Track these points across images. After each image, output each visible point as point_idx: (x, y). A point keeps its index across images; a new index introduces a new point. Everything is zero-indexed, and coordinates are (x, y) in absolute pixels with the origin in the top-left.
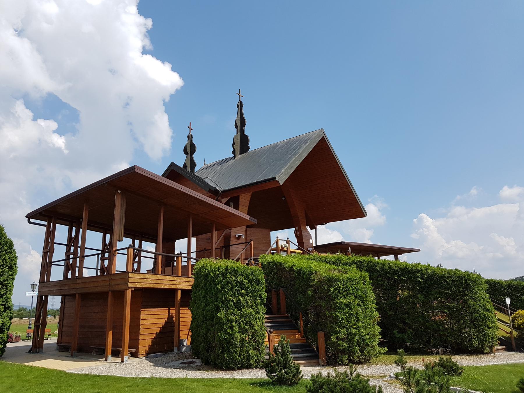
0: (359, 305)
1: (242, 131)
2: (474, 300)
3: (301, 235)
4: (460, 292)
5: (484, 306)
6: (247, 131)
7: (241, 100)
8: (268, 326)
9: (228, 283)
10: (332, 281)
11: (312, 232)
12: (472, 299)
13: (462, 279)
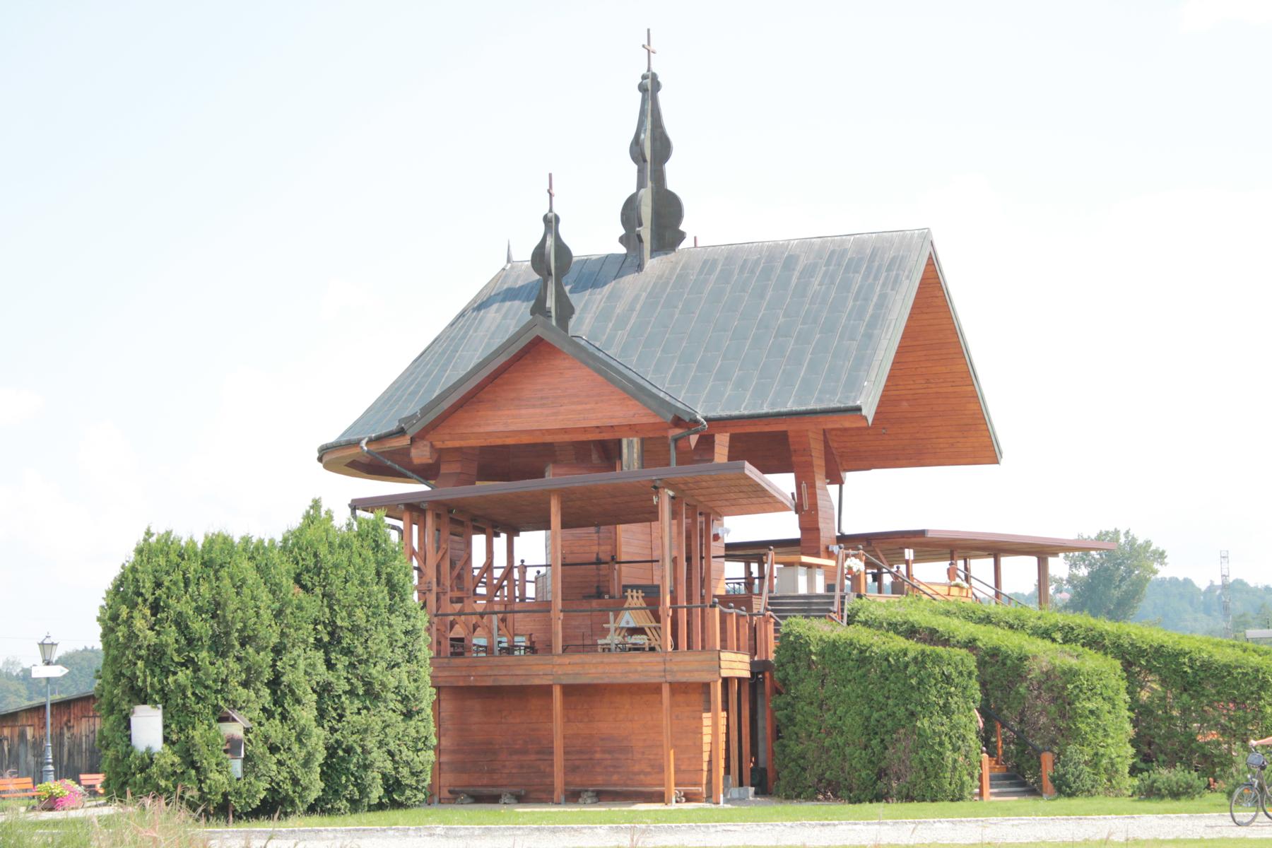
0: (1109, 712)
1: (659, 178)
3: (814, 506)
6: (676, 177)
7: (654, 69)
8: (646, 774)
9: (929, 676)
10: (1072, 674)
11: (833, 489)
13: (1257, 671)
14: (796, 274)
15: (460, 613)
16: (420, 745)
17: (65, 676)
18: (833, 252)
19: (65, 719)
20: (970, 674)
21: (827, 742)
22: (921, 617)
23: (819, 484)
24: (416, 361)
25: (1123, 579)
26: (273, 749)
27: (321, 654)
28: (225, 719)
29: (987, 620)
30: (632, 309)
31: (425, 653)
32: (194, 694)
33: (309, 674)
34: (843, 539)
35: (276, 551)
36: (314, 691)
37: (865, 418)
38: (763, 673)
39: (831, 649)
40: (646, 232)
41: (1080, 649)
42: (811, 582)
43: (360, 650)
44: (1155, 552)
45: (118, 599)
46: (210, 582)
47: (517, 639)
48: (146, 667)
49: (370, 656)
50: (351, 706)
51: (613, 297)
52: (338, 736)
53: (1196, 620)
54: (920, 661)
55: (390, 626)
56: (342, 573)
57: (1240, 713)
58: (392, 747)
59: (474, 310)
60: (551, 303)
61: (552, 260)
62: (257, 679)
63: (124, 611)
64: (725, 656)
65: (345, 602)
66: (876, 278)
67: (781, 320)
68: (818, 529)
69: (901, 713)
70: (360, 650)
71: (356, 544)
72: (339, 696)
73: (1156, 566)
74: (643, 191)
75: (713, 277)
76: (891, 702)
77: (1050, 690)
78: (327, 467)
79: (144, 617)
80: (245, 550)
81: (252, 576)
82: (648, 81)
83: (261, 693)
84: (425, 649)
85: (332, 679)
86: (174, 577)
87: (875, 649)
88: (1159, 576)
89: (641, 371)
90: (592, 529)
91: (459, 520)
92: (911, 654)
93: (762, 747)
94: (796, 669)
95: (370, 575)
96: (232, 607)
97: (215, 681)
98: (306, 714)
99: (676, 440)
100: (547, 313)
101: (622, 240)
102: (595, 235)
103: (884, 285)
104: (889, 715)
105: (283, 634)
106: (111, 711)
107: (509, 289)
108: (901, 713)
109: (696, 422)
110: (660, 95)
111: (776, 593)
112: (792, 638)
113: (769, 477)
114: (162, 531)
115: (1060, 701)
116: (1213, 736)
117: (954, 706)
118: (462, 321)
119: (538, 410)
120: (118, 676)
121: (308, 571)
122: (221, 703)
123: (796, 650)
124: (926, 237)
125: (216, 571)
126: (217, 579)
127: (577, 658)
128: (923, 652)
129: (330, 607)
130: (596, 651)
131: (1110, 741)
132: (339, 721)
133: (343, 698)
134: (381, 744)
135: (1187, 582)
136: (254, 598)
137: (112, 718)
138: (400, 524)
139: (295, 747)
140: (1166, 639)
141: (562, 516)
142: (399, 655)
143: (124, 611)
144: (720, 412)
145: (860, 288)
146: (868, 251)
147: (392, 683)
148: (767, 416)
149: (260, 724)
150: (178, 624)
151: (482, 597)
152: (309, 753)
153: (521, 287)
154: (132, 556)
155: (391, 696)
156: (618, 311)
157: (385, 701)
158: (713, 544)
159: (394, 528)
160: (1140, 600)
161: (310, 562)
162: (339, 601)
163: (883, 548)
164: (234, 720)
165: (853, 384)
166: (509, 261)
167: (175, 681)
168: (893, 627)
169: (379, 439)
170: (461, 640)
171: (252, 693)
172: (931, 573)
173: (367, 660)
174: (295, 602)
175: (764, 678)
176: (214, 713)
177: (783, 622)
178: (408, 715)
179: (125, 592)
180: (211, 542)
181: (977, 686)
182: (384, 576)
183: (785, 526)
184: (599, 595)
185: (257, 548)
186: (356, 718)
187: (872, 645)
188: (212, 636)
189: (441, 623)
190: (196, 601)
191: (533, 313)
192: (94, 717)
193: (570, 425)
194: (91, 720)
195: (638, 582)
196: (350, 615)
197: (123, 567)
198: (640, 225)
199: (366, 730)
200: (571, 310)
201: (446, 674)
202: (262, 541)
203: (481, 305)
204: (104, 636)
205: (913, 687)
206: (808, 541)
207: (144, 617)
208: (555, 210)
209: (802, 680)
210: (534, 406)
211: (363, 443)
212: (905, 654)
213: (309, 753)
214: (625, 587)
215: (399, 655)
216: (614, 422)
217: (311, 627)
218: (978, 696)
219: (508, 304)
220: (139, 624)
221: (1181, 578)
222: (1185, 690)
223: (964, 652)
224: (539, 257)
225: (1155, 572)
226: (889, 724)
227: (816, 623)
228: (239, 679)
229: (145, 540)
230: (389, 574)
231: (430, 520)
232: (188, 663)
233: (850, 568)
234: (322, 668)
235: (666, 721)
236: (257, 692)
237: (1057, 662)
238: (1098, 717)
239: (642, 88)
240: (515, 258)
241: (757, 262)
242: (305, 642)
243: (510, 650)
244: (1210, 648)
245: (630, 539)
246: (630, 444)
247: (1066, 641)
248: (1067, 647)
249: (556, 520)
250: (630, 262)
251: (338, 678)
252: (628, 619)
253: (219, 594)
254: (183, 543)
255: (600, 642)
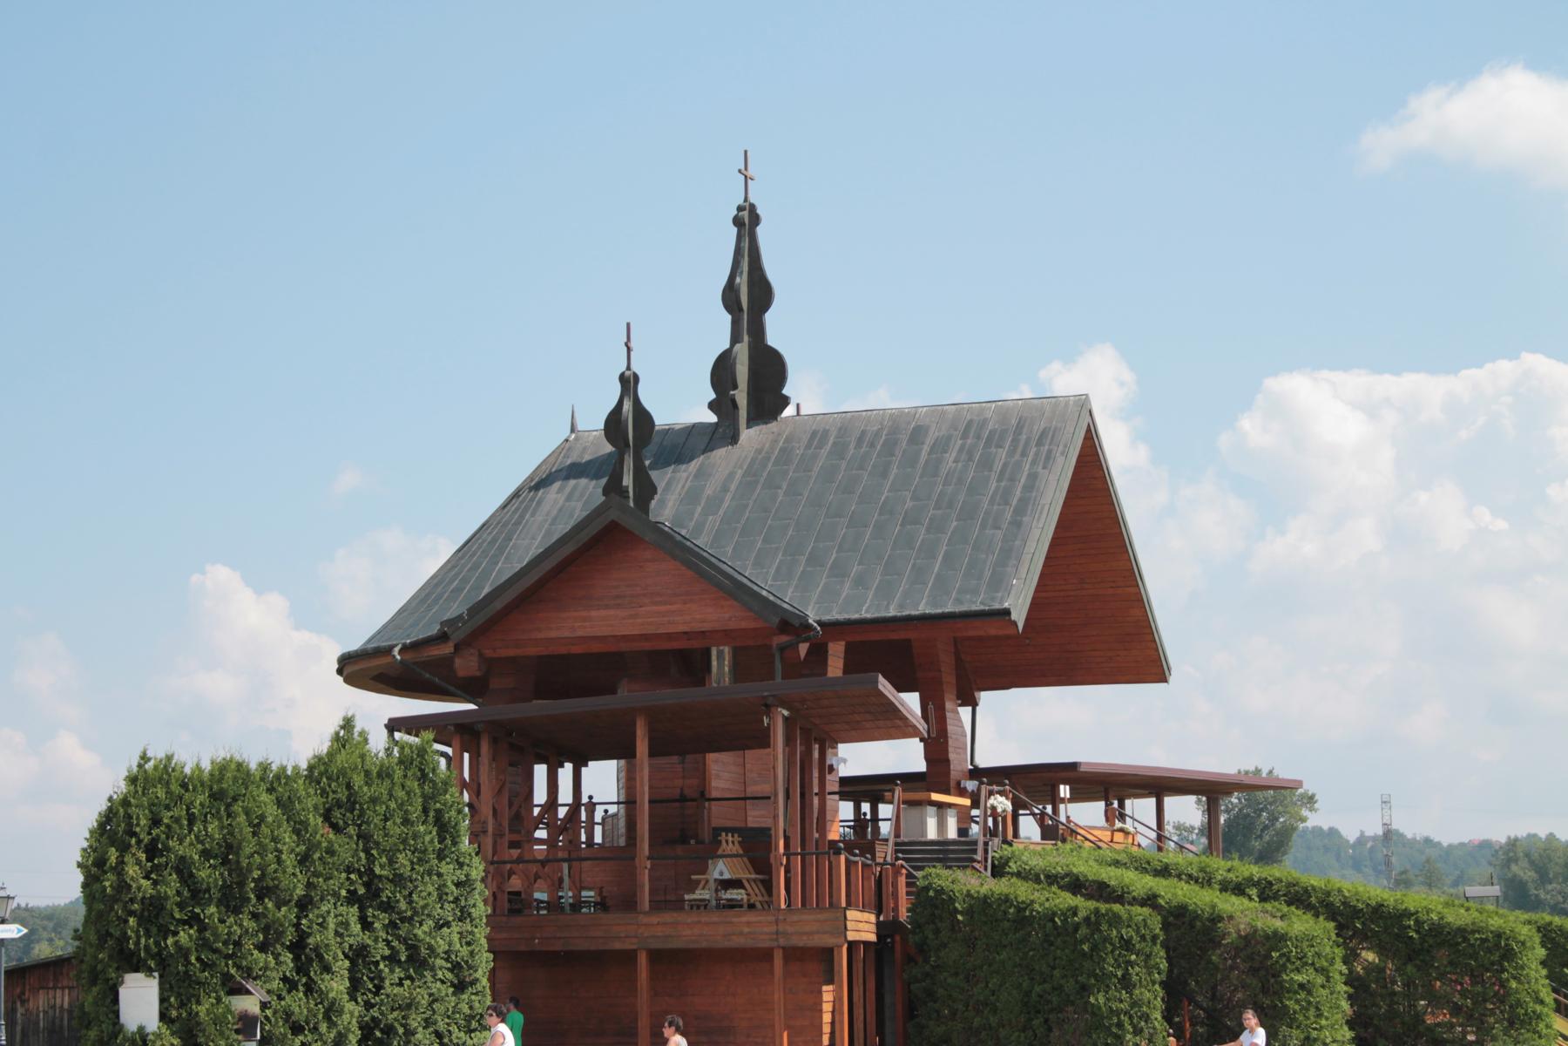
0: (1323, 986)
1: (758, 331)
2: (1519, 982)
4: (1493, 964)
5: (1536, 993)
6: (778, 330)
7: (752, 199)
10: (1277, 939)
11: (965, 713)
12: (1515, 978)
14: (926, 448)
15: (520, 860)
16: (474, 1024)
17: (21, 938)
18: (971, 422)
19: (18, 990)
20: (1154, 938)
21: (977, 1022)
22: (1086, 868)
23: (949, 705)
24: (459, 550)
25: (1266, 827)
26: (297, 1029)
27: (355, 910)
28: (241, 991)
29: (1164, 872)
30: (725, 489)
31: (481, 910)
32: (198, 959)
33: (341, 935)
34: (976, 773)
35: (301, 782)
36: (346, 956)
37: (1015, 624)
38: (891, 936)
39: (983, 906)
40: (741, 396)
41: (1285, 909)
42: (942, 825)
43: (403, 905)
44: (1302, 796)
45: (104, 840)
46: (220, 819)
47: (584, 893)
48: (139, 925)
49: (415, 913)
50: (391, 975)
51: (700, 474)
52: (375, 1012)
53: (1343, 876)
54: (1094, 921)
55: (440, 875)
56: (381, 809)
57: (1479, 988)
58: (441, 1026)
59: (531, 489)
60: (628, 481)
61: (630, 427)
62: (277, 940)
63: (113, 855)
64: (851, 914)
65: (387, 844)
66: (1024, 454)
67: (909, 504)
68: (948, 761)
69: (1070, 986)
70: (403, 905)
71: (398, 773)
72: (377, 963)
73: (1305, 812)
74: (738, 346)
75: (824, 452)
76: (1057, 973)
77: (1250, 958)
78: (350, 680)
79: (138, 862)
80: (262, 779)
81: (272, 812)
82: (745, 214)
83: (282, 959)
84: (481, 905)
85: (369, 942)
86: (176, 812)
87: (1036, 906)
88: (1309, 824)
89: (738, 565)
90: (675, 759)
91: (513, 745)
92: (1082, 914)
93: (889, 1028)
94: (937, 932)
95: (415, 812)
96: (248, 850)
97: (225, 943)
98: (337, 986)
99: (782, 649)
100: (623, 492)
101: (712, 406)
102: (680, 402)
103: (1034, 462)
104: (1054, 989)
105: (309, 885)
106: (93, 981)
107: (573, 465)
108: (1070, 986)
109: (809, 627)
110: (760, 230)
111: (903, 839)
112: (931, 893)
113: (903, 695)
114: (161, 755)
115: (1262, 973)
116: (1443, 1017)
117: (1135, 978)
118: (516, 503)
119: (612, 612)
120: (104, 936)
121: (340, 807)
122: (233, 971)
123: (936, 907)
124: (1083, 405)
125: (228, 806)
126: (229, 816)
127: (668, 917)
128: (1097, 911)
129: (367, 851)
130: (682, 908)
131: (1324, 1022)
132: (376, 994)
133: (381, 966)
134: (428, 1023)
135: (1333, 832)
136: (275, 840)
137: (95, 990)
138: (449, 750)
139: (323, 1027)
140: (1386, 896)
141: (651, 740)
142: (448, 912)
143: (113, 855)
144: (835, 615)
145: (1005, 465)
146: (1014, 422)
147: (442, 945)
148: (894, 620)
149: (280, 998)
150: (179, 871)
151: (541, 841)
152: (339, 1033)
153: (590, 462)
154: (123, 787)
155: (439, 962)
156: (708, 492)
157: (433, 969)
158: (828, 777)
159: (444, 754)
160: (1285, 853)
161: (342, 795)
162: (377, 844)
163: (1035, 783)
164: (248, 992)
165: (998, 583)
166: (573, 430)
167: (176, 943)
168: (1052, 879)
169: (416, 646)
170: (518, 893)
171: (271, 958)
172: (1087, 814)
173: (411, 918)
174: (324, 845)
175: (893, 942)
176: (223, 984)
177: (919, 874)
178: (460, 987)
179: (113, 830)
180: (222, 768)
181: (1163, 953)
182: (432, 814)
183: (907, 755)
184: (684, 840)
185: (278, 777)
186: (397, 990)
187: (1032, 902)
188: (224, 886)
189: (497, 871)
190: (202, 843)
191: (606, 491)
192: (55, 988)
193: (651, 630)
194: (51, 993)
195: (729, 824)
196: (391, 862)
197: (110, 799)
198: (735, 387)
199: (409, 1006)
200: (654, 490)
201: (504, 935)
202: (284, 769)
203: (539, 483)
204: (85, 886)
205: (1084, 954)
206: (938, 774)
207: (138, 862)
208: (634, 368)
209: (945, 946)
210: (607, 607)
211: (396, 651)
212: (1075, 914)
213: (339, 1033)
214: (717, 831)
215: (448, 912)
216: (706, 627)
217: (344, 875)
218: (1164, 965)
219: (572, 482)
220: (132, 870)
221: (1325, 828)
222: (1410, 959)
223: (1146, 911)
224: (614, 423)
225: (1303, 820)
226: (1055, 1000)
227: (959, 874)
228: (255, 940)
229: (140, 766)
230: (438, 811)
231: (485, 748)
232: (193, 920)
233: (994, 808)
234: (356, 928)
235: (778, 996)
236: (276, 956)
237: (1259, 925)
238: (1309, 993)
239: (737, 221)
240: (580, 427)
241: (877, 434)
242: (336, 895)
243: (577, 906)
244: (1440, 907)
245: (722, 771)
246: (720, 655)
247: (1263, 898)
248: (1268, 906)
249: (642, 747)
250: (723, 432)
251: (376, 940)
252: (721, 869)
253: (231, 834)
254: (187, 770)
255: (687, 897)
